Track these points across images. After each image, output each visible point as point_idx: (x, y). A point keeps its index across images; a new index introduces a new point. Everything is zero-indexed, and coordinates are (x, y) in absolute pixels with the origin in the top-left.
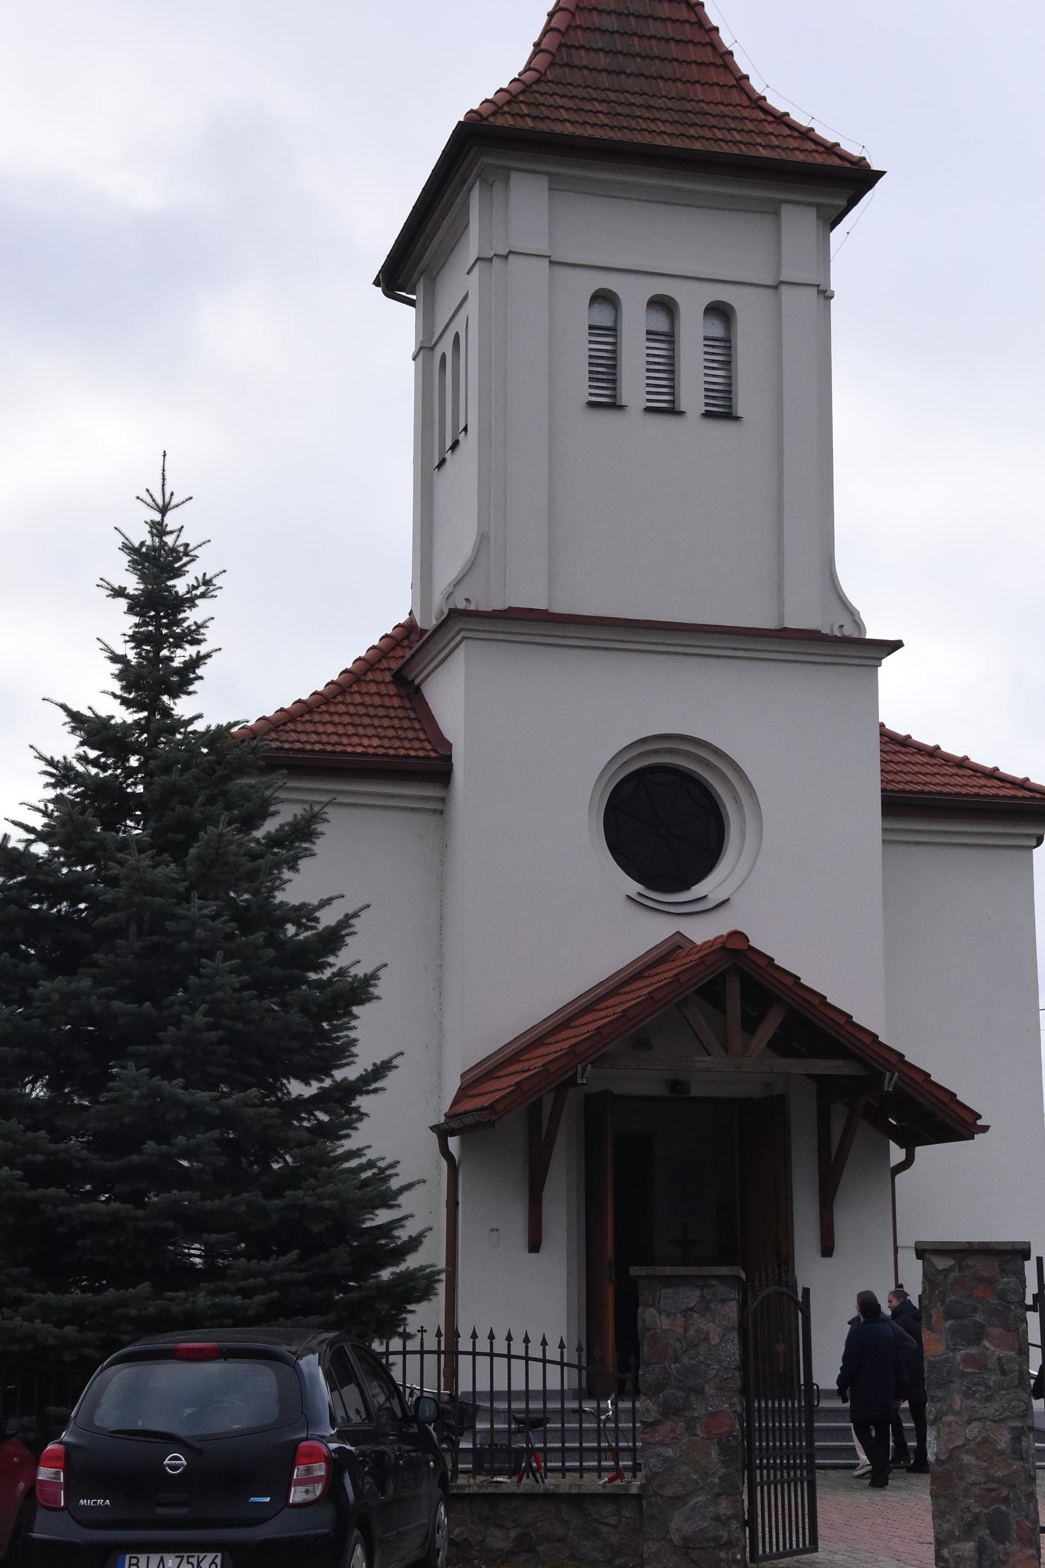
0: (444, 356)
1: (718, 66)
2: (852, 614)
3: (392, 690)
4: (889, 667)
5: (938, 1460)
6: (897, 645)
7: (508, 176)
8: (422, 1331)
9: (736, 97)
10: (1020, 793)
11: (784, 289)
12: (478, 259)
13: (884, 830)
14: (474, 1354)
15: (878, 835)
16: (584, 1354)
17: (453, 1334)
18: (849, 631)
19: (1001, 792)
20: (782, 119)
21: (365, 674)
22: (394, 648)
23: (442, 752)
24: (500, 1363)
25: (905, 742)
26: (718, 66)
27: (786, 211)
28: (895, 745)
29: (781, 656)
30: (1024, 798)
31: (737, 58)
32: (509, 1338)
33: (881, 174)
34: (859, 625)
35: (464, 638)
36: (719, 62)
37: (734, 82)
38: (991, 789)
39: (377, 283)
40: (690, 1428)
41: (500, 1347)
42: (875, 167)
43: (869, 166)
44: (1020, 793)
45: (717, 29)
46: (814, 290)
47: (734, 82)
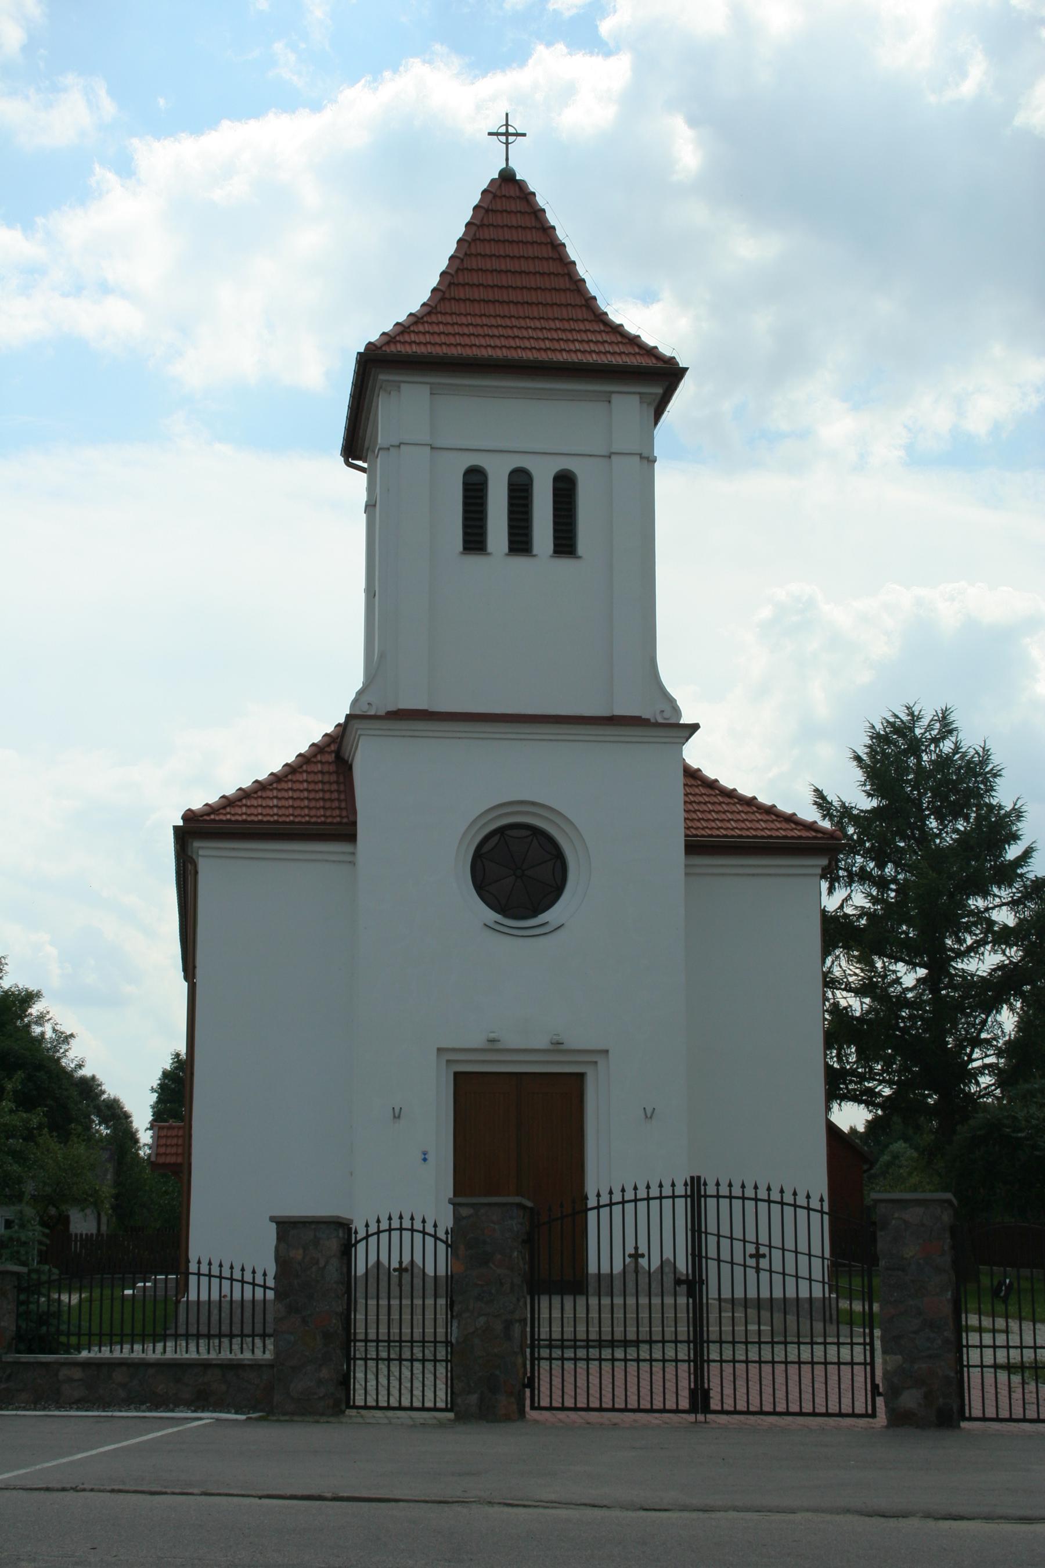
1: (538, 229)
2: (671, 702)
5: (457, 1341)
7: (399, 387)
9: (520, 206)
14: (718, 1197)
15: (682, 870)
16: (689, 1188)
18: (669, 717)
19: (790, 834)
24: (215, 1282)
25: (712, 785)
26: (538, 229)
27: (615, 398)
28: (692, 775)
30: (808, 838)
34: (677, 711)
36: (573, 287)
37: (584, 302)
43: (678, 364)
46: (638, 458)
47: (584, 302)
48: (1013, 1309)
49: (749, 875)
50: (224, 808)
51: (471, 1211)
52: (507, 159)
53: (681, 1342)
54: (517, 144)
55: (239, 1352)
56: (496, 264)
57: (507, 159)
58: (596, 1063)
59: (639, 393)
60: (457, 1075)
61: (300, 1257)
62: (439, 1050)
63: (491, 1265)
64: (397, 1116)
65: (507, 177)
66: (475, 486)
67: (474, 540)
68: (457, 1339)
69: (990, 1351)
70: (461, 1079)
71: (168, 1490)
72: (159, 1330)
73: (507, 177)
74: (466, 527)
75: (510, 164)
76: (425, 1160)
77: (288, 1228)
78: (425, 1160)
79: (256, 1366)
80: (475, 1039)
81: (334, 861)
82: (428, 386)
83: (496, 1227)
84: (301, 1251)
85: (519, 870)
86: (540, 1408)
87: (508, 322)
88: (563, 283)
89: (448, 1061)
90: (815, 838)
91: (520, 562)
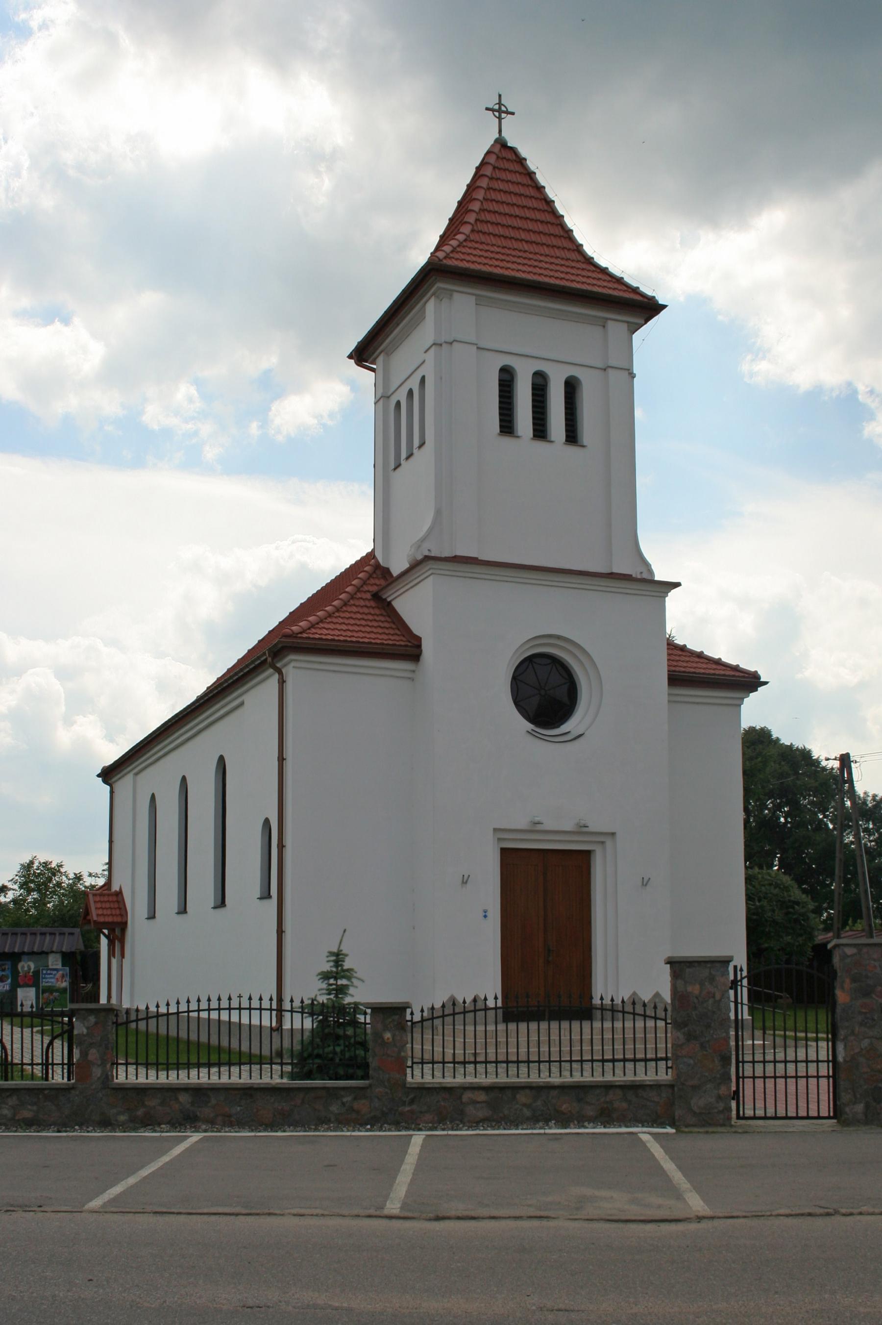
0: (398, 404)
3: (373, 604)
4: (672, 599)
5: (845, 1061)
6: (678, 585)
7: (451, 295)
8: (240, 997)
10: (737, 674)
11: (610, 371)
12: (434, 344)
13: (669, 695)
15: (665, 697)
17: (280, 1000)
18: (645, 576)
19: (717, 672)
20: (604, 271)
21: (355, 594)
22: (369, 579)
23: (416, 643)
27: (610, 324)
29: (644, 593)
30: (739, 677)
31: (575, 233)
32: (261, 999)
33: (664, 307)
34: (651, 572)
35: (432, 574)
36: (566, 235)
38: (711, 670)
39: (350, 357)
40: (703, 1047)
41: (235, 1004)
42: (660, 302)
44: (737, 674)
45: (563, 216)
48: (297, 1038)
49: (694, 703)
50: (309, 629)
51: (853, 951)
52: (500, 131)
53: (522, 1062)
54: (507, 120)
55: (567, 1073)
56: (507, 209)
57: (500, 131)
58: (603, 843)
59: (628, 322)
60: (503, 851)
61: (697, 992)
62: (495, 830)
63: (874, 996)
64: (464, 882)
65: (501, 143)
66: (507, 381)
67: (507, 426)
68: (844, 1058)
69: (771, 1065)
70: (506, 854)
71: (855, 1211)
72: (183, 1059)
73: (501, 143)
74: (566, 403)
75: (503, 134)
76: (485, 916)
77: (679, 967)
78: (485, 916)
79: (657, 1086)
80: (522, 823)
81: (397, 677)
82: (474, 297)
83: (877, 964)
84: (697, 987)
85: (546, 692)
86: (745, 1118)
87: (525, 255)
88: (558, 231)
89: (499, 839)
90: (744, 677)
91: (540, 445)
